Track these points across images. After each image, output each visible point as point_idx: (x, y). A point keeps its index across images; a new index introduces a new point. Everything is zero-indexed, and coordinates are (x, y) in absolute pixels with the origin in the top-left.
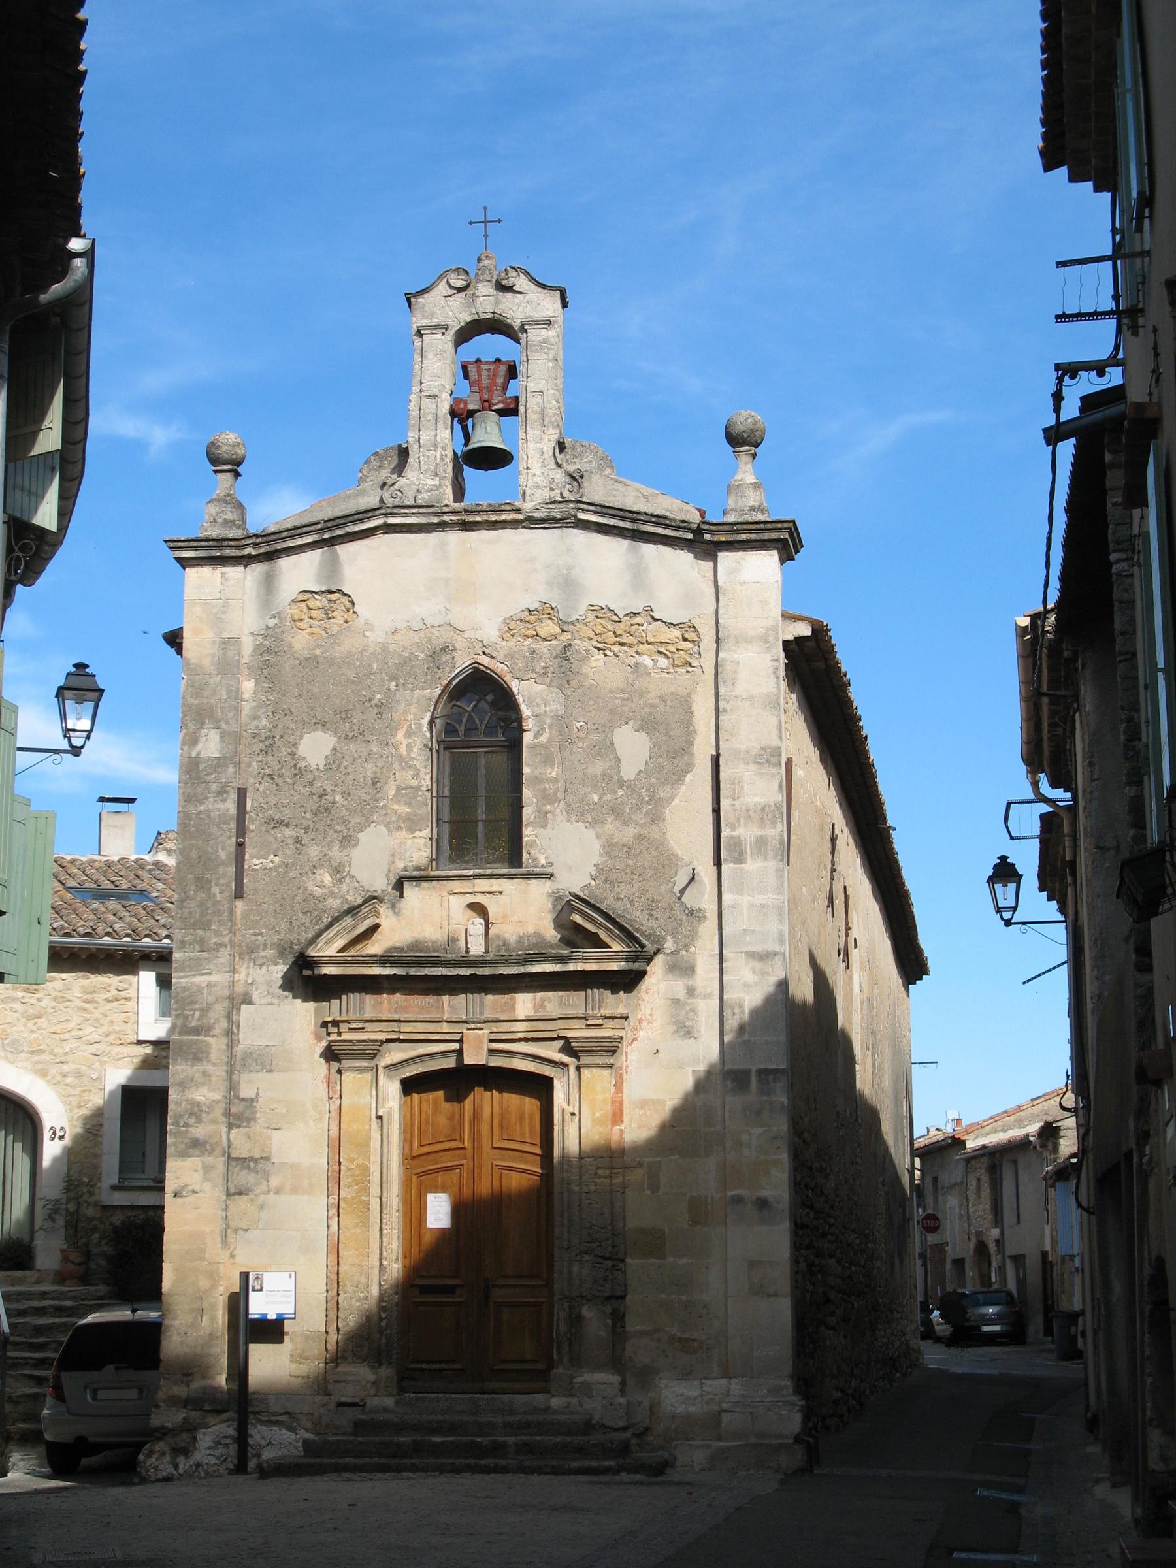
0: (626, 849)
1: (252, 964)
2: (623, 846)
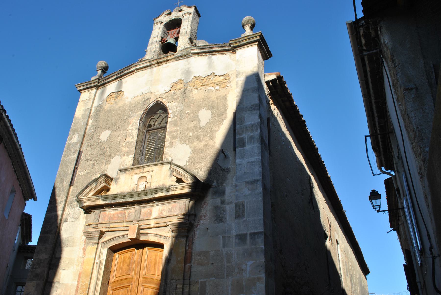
0: (200, 150)
1: (70, 208)
2: (199, 149)
